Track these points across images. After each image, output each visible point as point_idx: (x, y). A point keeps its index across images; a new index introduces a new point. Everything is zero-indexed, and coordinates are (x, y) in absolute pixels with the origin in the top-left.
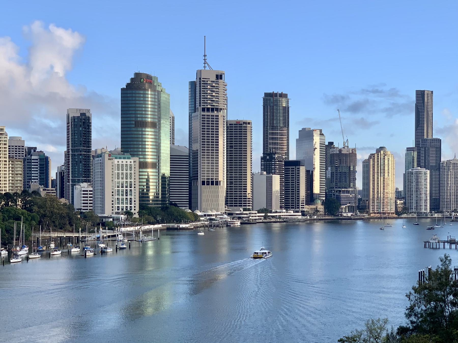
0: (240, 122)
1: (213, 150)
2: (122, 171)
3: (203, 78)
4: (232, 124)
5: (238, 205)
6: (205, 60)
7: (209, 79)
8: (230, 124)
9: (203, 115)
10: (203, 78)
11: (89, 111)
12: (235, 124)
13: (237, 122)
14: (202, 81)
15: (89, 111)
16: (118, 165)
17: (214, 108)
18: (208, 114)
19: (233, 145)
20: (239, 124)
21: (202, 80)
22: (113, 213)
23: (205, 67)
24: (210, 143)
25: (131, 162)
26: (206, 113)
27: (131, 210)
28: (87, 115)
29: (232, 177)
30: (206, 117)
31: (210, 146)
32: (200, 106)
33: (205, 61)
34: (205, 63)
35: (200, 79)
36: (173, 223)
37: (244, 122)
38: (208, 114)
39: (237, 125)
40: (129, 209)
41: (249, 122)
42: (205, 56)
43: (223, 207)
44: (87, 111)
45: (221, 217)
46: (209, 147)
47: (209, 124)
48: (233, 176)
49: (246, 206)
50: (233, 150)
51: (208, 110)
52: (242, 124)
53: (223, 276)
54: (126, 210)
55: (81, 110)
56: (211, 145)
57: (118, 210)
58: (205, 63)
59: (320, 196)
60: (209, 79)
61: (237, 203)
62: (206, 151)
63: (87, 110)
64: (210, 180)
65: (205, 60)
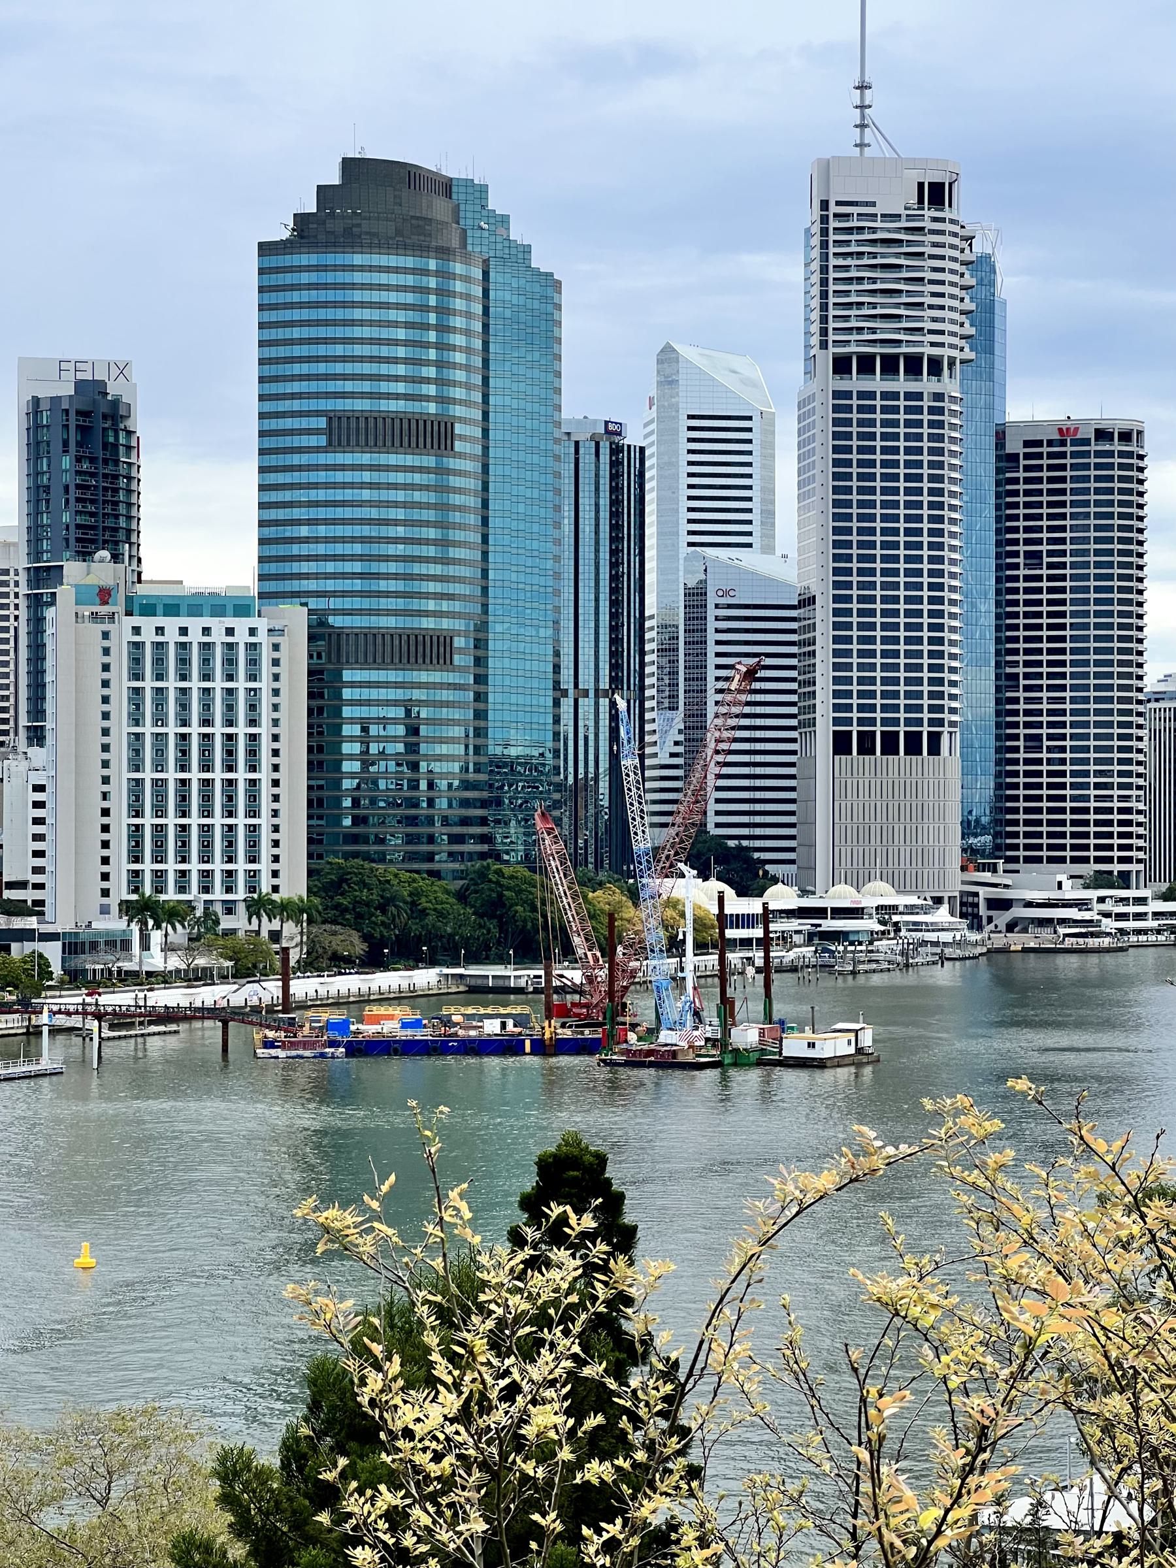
0: (1076, 429)
1: (896, 572)
2: (184, 677)
3: (838, 203)
4: (1039, 443)
5: (1068, 854)
6: (862, 107)
7: (873, 204)
8: (1027, 444)
9: (837, 394)
10: (838, 203)
11: (123, 370)
12: (1050, 443)
13: (1060, 430)
14: (835, 215)
15: (123, 370)
16: (183, 646)
17: (896, 357)
18: (890, 386)
19: (1044, 548)
20: (1075, 443)
21: (833, 209)
22: (105, 910)
23: (861, 145)
24: (878, 538)
25: (253, 632)
26: (855, 383)
27: (159, 890)
28: (112, 390)
29: (1039, 713)
30: (878, 403)
31: (878, 552)
32: (824, 345)
33: (863, 117)
34: (862, 126)
35: (825, 205)
36: (502, 960)
37: (1097, 430)
38: (890, 386)
39: (1063, 443)
40: (148, 891)
41: (1126, 426)
42: (862, 87)
43: (960, 876)
44: (115, 372)
45: (915, 923)
46: (872, 559)
47: (872, 436)
48: (1045, 706)
49: (1109, 860)
50: (1045, 572)
51: (866, 365)
52: (1086, 442)
53: (350, 1303)
54: (252, 889)
55: (64, 366)
56: (885, 545)
57: (229, 890)
58: (862, 126)
59: (485, 795)
60: (873, 204)
61: (1062, 847)
62: (855, 579)
63: (113, 366)
64: (878, 729)
65: (862, 107)
